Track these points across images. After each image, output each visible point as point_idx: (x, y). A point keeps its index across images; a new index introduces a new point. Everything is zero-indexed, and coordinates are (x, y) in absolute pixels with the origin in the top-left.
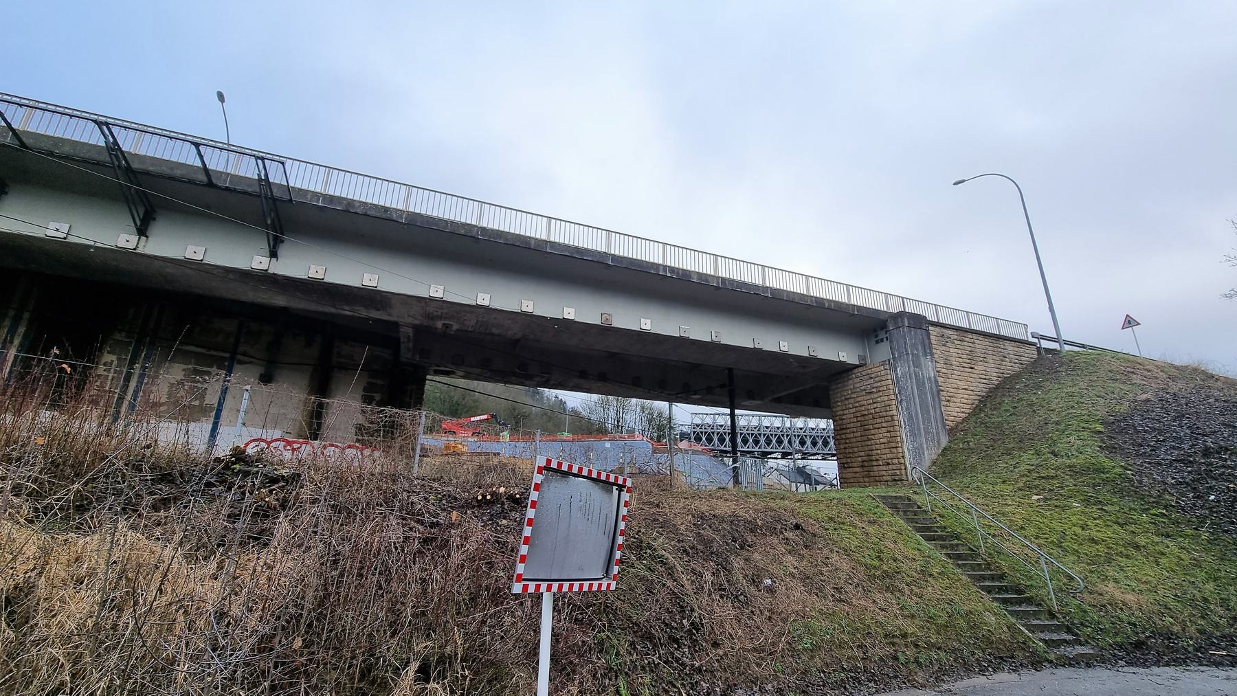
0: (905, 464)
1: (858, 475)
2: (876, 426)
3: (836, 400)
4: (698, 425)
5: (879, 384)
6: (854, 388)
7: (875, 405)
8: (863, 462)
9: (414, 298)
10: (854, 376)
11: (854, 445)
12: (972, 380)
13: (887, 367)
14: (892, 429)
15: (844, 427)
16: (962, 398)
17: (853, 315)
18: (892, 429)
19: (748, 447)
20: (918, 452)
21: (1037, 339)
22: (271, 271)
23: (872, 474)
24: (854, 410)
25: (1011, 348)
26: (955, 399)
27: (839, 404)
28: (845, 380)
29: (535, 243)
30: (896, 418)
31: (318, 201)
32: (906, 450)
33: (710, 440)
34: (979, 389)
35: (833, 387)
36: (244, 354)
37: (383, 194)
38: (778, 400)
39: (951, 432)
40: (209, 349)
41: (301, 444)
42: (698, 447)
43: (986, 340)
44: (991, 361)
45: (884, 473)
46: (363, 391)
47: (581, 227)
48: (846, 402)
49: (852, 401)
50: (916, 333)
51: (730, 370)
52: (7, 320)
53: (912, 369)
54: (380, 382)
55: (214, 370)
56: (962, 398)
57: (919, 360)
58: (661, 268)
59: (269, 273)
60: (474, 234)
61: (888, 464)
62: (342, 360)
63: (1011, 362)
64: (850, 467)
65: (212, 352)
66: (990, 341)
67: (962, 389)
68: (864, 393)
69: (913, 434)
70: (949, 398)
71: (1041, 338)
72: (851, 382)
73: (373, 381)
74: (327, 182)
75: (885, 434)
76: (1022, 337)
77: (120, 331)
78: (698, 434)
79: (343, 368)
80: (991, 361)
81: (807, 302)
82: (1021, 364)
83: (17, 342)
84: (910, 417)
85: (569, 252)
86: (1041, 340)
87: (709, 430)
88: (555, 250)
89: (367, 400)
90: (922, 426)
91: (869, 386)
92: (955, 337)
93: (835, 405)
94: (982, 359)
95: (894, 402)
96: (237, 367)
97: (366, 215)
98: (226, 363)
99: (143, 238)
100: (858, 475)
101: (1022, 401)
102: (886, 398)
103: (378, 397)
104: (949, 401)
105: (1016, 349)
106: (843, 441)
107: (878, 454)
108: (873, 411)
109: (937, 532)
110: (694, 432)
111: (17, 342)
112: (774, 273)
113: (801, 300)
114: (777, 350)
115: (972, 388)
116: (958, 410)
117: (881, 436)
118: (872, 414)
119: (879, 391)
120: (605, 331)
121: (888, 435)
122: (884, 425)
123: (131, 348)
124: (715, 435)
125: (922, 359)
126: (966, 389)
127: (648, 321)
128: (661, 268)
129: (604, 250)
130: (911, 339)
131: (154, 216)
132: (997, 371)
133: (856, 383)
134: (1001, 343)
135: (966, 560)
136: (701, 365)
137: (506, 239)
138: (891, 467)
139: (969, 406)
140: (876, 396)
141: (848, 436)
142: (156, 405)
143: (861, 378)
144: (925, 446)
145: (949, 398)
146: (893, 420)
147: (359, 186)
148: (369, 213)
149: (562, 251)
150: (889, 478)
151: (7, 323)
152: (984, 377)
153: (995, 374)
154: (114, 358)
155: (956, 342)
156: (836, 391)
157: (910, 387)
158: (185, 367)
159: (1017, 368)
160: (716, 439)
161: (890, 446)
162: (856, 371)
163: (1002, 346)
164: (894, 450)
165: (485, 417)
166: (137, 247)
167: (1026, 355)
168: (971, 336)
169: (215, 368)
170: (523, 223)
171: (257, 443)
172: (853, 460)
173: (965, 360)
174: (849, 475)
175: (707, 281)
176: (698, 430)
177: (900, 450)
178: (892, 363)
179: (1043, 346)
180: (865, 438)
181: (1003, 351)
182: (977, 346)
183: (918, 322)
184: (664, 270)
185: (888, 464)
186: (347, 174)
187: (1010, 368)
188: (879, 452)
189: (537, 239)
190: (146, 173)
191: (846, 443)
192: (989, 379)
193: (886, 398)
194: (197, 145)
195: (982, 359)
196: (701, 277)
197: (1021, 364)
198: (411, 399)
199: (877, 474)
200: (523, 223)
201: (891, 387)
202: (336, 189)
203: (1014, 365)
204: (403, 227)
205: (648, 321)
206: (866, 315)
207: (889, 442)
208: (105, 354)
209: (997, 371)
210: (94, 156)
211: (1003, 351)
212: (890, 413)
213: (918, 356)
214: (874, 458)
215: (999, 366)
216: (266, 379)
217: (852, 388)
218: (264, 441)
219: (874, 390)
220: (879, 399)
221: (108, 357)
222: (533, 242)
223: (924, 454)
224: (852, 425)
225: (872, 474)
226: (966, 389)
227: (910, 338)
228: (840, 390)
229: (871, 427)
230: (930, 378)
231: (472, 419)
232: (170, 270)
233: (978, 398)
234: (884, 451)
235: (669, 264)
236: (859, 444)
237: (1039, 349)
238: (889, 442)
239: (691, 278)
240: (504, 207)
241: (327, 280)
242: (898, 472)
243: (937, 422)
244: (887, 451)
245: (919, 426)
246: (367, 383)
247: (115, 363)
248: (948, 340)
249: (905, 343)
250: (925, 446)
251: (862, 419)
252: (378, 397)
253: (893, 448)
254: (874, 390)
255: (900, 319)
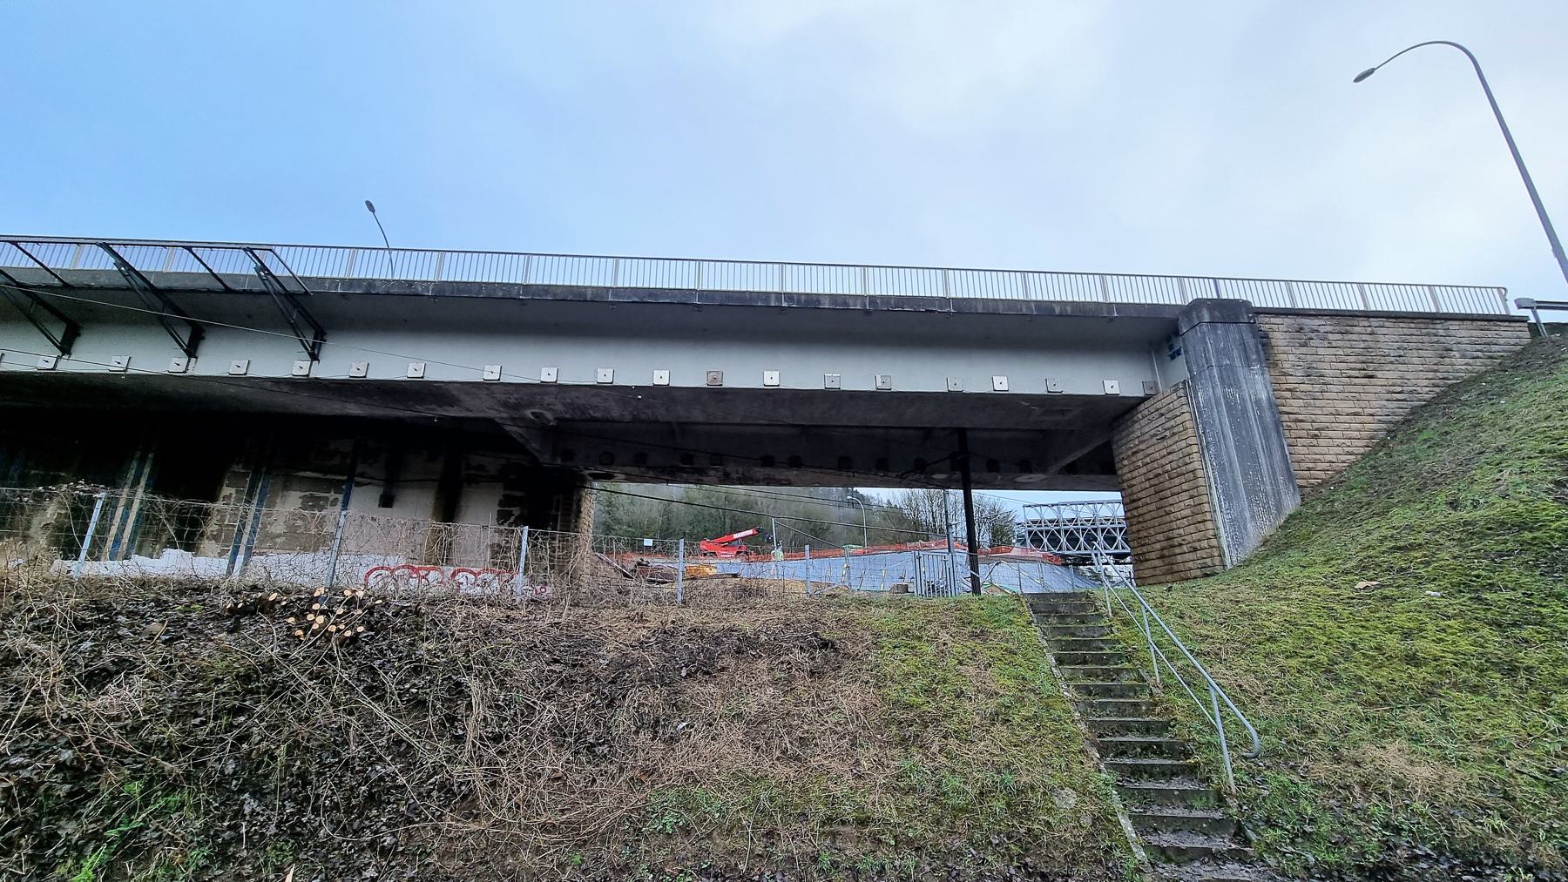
0: (1219, 547)
1: (1158, 572)
2: (1175, 490)
3: (1121, 457)
4: (1051, 521)
5: (1172, 423)
6: (1143, 434)
7: (1171, 457)
8: (1162, 549)
9: (471, 385)
10: (1139, 416)
11: (1149, 524)
12: (1371, 396)
13: (1181, 393)
14: (1194, 492)
15: (1135, 497)
16: (1347, 429)
17: (1112, 319)
18: (1194, 492)
19: (1116, 548)
20: (1237, 524)
21: (1530, 310)
22: (312, 376)
23: (1175, 568)
24: (1143, 470)
25: (1463, 333)
26: (1331, 433)
27: (1126, 462)
28: (1129, 423)
29: (592, 294)
30: (1200, 473)
31: (337, 289)
32: (1221, 525)
33: (1054, 541)
34: (1386, 411)
35: (1116, 439)
36: (362, 475)
37: (660, 276)
38: (1071, 469)
39: (1308, 494)
40: (326, 473)
41: (429, 570)
42: (1038, 553)
43: (1401, 325)
44: (1415, 360)
45: (1190, 565)
46: (499, 505)
47: (994, 273)
48: (1134, 459)
49: (1140, 455)
50: (1227, 331)
51: (961, 432)
52: (134, 462)
53: (1219, 390)
54: (518, 494)
55: (332, 495)
56: (1347, 429)
57: (1235, 373)
58: (773, 297)
59: (311, 379)
60: (514, 294)
61: (1195, 550)
62: (473, 472)
63: (1463, 357)
64: (1147, 560)
65: (329, 477)
66: (1413, 325)
67: (1348, 415)
68: (1154, 440)
69: (1228, 498)
70: (1317, 432)
71: (1538, 308)
72: (1137, 426)
73: (507, 492)
74: (77, 257)
75: (1187, 502)
76: (1500, 310)
77: (238, 464)
78: (1109, 532)
79: (474, 481)
80: (1415, 360)
81: (1021, 310)
82: (1490, 357)
83: (143, 483)
84: (1222, 470)
85: (638, 297)
86: (1538, 311)
87: (1052, 528)
88: (618, 297)
89: (503, 517)
90: (1240, 482)
91: (1160, 429)
92: (1329, 328)
93: (1120, 465)
94: (1393, 359)
95: (1195, 449)
96: (356, 491)
97: (388, 294)
98: (344, 487)
99: (193, 360)
100: (1158, 572)
101: (1464, 420)
102: (1183, 444)
103: (516, 511)
104: (1316, 437)
105: (1479, 333)
106: (1135, 520)
107: (1181, 536)
108: (1168, 467)
109: (1102, 649)
110: (1030, 533)
111: (143, 483)
112: (1468, 294)
113: (1010, 309)
114: (1043, 391)
115: (1371, 411)
116: (1339, 450)
117: (1181, 506)
118: (1167, 472)
119: (1174, 434)
120: (718, 395)
121: (1191, 502)
122: (1185, 487)
123: (248, 479)
124: (1099, 532)
125: (1241, 372)
126: (1355, 414)
127: (1004, 380)
128: (773, 297)
129: (941, 295)
130: (1216, 341)
131: (325, 338)
132: (1431, 375)
133: (1144, 426)
134: (1438, 326)
135: (1122, 697)
136: (933, 428)
137: (555, 295)
138: (1199, 554)
139: (1363, 442)
140: (1170, 442)
141: (1141, 511)
142: (274, 537)
143: (1150, 417)
144: (1248, 515)
145: (1317, 432)
146: (1196, 478)
147: (660, 270)
148: (392, 291)
149: (629, 297)
150: (1198, 573)
151: (134, 464)
152: (1399, 389)
153: (1426, 382)
154: (233, 491)
155: (1331, 336)
156: (1120, 443)
157: (1217, 422)
158: (303, 494)
159: (1478, 366)
160: (1063, 539)
161: (1195, 521)
162: (1142, 407)
163: (1441, 332)
164: (1201, 526)
165: (750, 532)
166: (187, 369)
167: (1502, 341)
168: (1366, 324)
169: (332, 493)
170: (896, 283)
171: (379, 572)
172: (1150, 548)
173: (1353, 365)
174: (1147, 573)
175: (845, 303)
176: (1035, 528)
177: (1209, 525)
178: (1188, 388)
179: (1543, 321)
180: (1161, 512)
181: (1442, 339)
182: (1382, 338)
183: (1229, 312)
184: (777, 298)
185: (1195, 550)
186: (691, 262)
187: (1459, 366)
188: (1181, 531)
189: (1149, 304)
190: (171, 290)
191: (1140, 522)
192: (1411, 392)
193: (1183, 444)
194: (189, 249)
195: (1393, 359)
196: (836, 301)
197: (1490, 357)
198: (557, 510)
199: (1181, 567)
200: (896, 283)
201: (1189, 424)
202: (537, 278)
203: (1471, 361)
204: (435, 302)
205: (1004, 380)
206: (1136, 315)
207: (1194, 514)
208: (225, 487)
209: (1431, 375)
210: (104, 281)
211: (1442, 339)
212: (1190, 467)
213: (1231, 368)
214: (1176, 542)
215: (1435, 367)
216: (387, 501)
217: (1139, 434)
218: (388, 569)
219: (1167, 433)
220: (1174, 447)
221: (227, 491)
222: (589, 292)
223: (1245, 529)
224: (1143, 494)
225: (1175, 568)
226: (1355, 414)
227: (1205, 341)
228: (1124, 441)
229: (1168, 493)
230: (1258, 402)
231: (736, 536)
232: (680, 413)
233: (1384, 426)
234: (1188, 530)
235: (1112, 300)
236: (1155, 522)
237: (1534, 329)
238: (1194, 514)
239: (819, 304)
240: (927, 268)
241: (369, 377)
242: (1208, 561)
243: (1274, 473)
244: (1192, 529)
245: (1235, 482)
246: (504, 496)
247: (234, 495)
248: (1312, 335)
249: (1205, 350)
250: (1248, 515)
251: (1155, 481)
252: (516, 511)
253: (1199, 522)
254: (1167, 433)
255: (1194, 313)
